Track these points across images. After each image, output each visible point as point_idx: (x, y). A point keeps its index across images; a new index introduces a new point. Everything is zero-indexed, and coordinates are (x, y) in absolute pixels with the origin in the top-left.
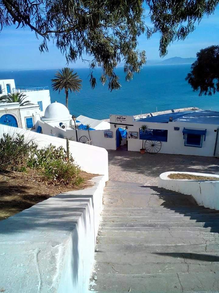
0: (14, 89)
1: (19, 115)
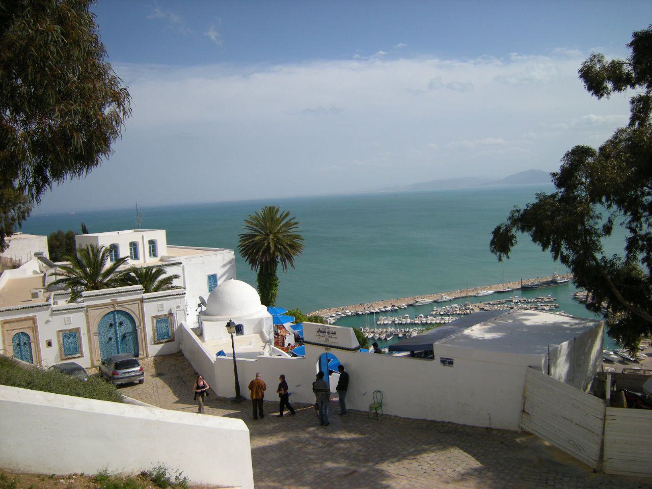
1: (141, 314)
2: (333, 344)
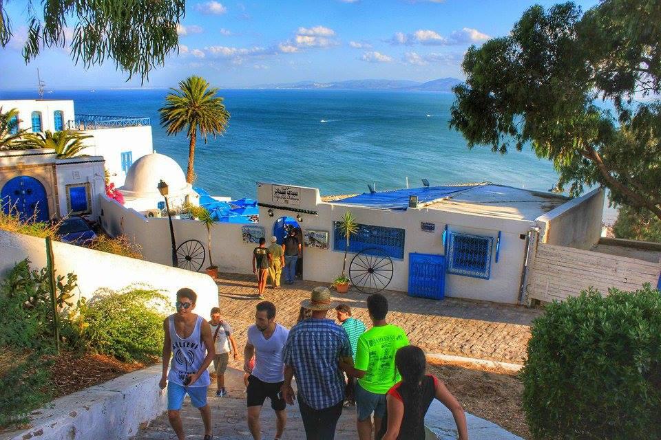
0: (71, 122)
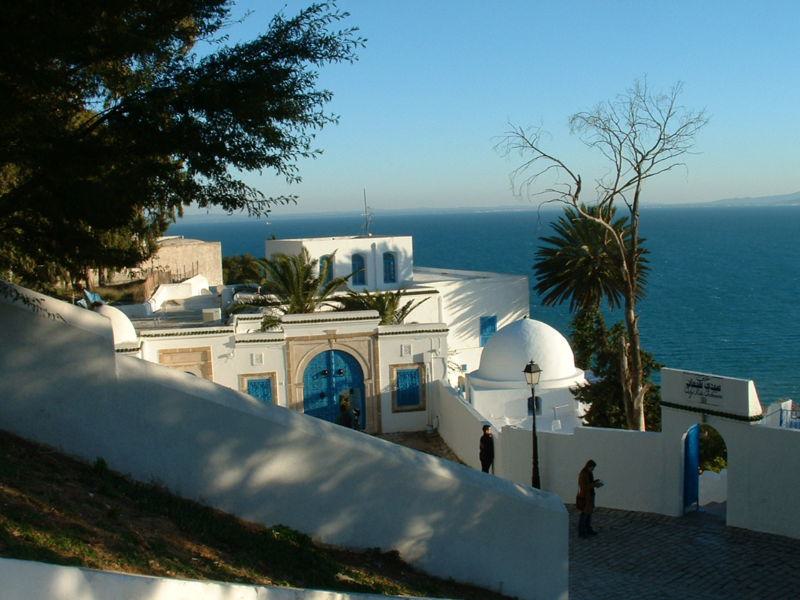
2: (715, 409)
